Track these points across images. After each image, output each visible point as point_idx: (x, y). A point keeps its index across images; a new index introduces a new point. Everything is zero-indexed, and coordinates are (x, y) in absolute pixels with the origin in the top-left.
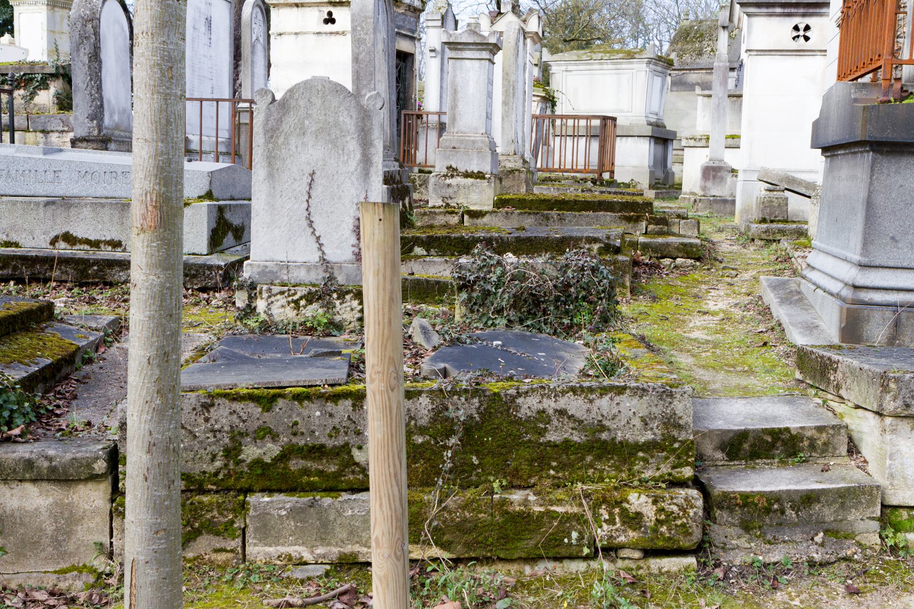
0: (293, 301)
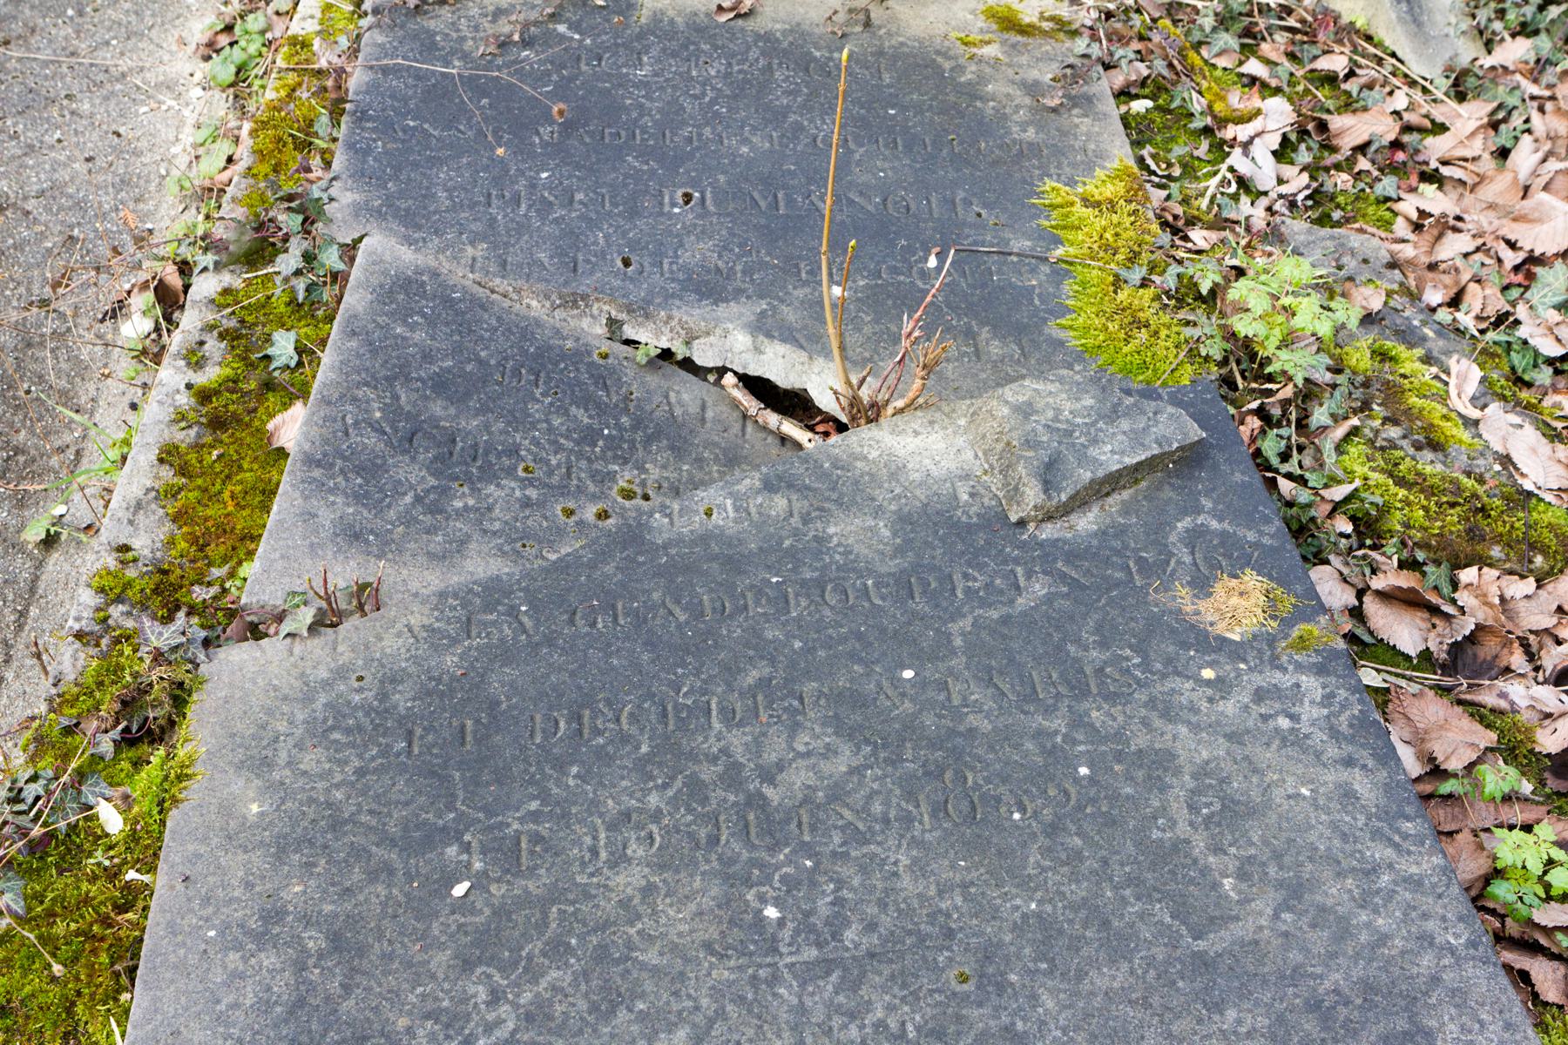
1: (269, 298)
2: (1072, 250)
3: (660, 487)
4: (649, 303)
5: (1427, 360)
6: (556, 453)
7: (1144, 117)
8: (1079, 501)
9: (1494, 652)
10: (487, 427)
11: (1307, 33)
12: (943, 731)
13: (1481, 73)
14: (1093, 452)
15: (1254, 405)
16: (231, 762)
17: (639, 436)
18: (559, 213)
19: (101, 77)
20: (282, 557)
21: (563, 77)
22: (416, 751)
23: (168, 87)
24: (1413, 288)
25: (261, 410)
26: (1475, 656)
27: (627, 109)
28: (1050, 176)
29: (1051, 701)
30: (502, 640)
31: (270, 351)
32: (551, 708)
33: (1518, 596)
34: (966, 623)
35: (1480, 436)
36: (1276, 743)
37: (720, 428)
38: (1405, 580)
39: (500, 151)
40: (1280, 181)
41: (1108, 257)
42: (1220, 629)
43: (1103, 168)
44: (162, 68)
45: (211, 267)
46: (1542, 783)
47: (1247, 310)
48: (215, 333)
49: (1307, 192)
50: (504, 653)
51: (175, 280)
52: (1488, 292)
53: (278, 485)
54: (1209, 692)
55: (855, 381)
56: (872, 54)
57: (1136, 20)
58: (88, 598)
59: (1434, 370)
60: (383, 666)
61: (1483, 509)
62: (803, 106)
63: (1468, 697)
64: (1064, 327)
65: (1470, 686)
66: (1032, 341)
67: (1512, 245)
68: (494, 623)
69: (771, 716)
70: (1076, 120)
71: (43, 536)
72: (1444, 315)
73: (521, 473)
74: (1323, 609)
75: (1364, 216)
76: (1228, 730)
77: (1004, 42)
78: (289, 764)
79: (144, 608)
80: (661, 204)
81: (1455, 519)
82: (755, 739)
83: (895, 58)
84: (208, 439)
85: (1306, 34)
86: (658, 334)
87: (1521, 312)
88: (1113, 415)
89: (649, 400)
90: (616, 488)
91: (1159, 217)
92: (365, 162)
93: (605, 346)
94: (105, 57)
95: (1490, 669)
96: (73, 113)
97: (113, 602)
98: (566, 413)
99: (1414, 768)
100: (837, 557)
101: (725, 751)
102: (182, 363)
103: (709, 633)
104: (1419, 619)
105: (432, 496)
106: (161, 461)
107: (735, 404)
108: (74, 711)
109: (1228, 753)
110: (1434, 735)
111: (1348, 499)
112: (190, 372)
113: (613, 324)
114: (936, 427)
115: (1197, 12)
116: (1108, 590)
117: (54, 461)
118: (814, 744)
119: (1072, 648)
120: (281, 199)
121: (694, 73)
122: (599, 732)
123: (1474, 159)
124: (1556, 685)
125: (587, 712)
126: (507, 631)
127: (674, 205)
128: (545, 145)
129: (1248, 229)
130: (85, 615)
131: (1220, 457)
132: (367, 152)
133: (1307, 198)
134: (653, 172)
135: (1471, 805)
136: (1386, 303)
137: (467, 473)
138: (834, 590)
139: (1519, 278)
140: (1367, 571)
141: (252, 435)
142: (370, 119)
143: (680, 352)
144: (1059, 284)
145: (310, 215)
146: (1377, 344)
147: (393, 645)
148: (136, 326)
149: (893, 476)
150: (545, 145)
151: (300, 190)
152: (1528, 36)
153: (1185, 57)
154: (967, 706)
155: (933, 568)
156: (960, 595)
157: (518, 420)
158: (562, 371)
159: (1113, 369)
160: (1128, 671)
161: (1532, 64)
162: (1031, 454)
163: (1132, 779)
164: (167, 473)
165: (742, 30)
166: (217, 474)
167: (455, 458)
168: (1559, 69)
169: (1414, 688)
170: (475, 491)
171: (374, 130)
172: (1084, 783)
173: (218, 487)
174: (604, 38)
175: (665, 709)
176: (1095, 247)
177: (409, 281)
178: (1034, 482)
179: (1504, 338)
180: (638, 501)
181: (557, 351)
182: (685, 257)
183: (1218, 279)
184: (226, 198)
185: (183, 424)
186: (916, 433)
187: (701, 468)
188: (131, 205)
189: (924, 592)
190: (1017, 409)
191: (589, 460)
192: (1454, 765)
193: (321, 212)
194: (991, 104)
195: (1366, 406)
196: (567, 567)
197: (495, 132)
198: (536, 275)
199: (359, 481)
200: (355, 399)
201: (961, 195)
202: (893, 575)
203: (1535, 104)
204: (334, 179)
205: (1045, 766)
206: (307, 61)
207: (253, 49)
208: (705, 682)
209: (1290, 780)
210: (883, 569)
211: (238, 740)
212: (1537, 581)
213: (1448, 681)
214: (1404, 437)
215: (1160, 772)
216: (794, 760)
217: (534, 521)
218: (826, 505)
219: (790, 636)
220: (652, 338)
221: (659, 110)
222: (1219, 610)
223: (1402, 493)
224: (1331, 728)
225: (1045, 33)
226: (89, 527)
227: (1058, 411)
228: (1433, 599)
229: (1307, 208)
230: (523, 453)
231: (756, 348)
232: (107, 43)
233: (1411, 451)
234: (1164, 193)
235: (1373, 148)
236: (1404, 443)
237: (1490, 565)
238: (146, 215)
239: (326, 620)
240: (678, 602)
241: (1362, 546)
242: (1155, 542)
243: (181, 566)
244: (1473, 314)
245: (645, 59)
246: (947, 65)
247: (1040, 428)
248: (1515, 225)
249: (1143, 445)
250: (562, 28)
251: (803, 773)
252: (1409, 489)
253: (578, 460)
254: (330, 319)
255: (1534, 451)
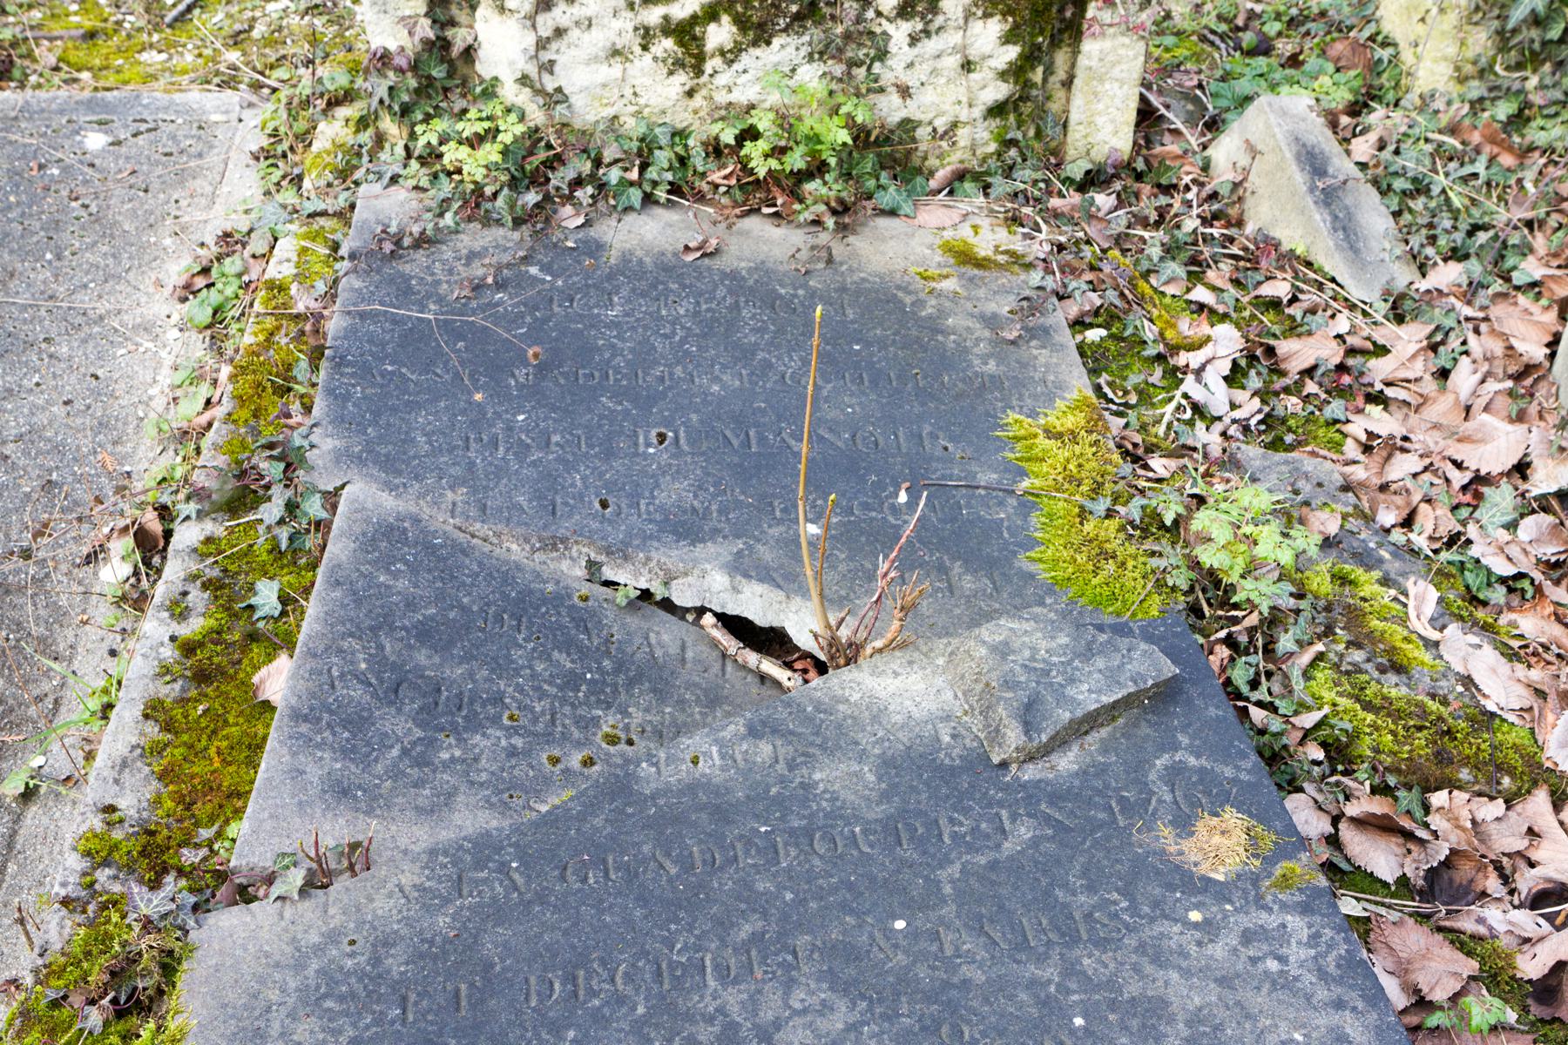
0: (670, 28)
1: (251, 546)
2: (1038, 483)
3: (643, 731)
4: (628, 545)
5: (1385, 582)
6: (540, 699)
7: (1100, 346)
8: (1059, 742)
9: (1469, 876)
10: (471, 675)
11: (1251, 260)
12: (937, 984)
13: (1417, 297)
14: (1070, 691)
15: (1222, 634)
16: (222, 1035)
17: (621, 678)
18: (536, 455)
19: (80, 320)
20: (271, 816)
21: (536, 319)
22: (411, 1018)
23: (145, 329)
24: (1367, 511)
25: (246, 662)
26: (1451, 880)
27: (599, 349)
28: (1012, 408)
29: (1041, 949)
30: (494, 899)
31: (253, 601)
32: (545, 970)
33: (1489, 818)
34: (955, 870)
35: (1441, 657)
36: (1266, 987)
37: (700, 668)
38: (1378, 806)
39: (478, 397)
40: (1233, 406)
41: (1072, 488)
42: (1204, 869)
43: (1064, 399)
44: (139, 311)
45: (194, 516)
46: (1525, 1009)
47: (1210, 540)
48: (198, 583)
49: (1260, 417)
50: (497, 913)
51: (155, 526)
52: (1439, 512)
53: (265, 739)
54: (1198, 935)
55: (833, 623)
56: (836, 290)
57: (1087, 252)
58: (75, 862)
59: (1393, 592)
60: (375, 929)
61: (1449, 732)
62: (771, 343)
63: (1447, 924)
64: (1033, 560)
65: (1449, 912)
66: (1004, 574)
67: (1459, 465)
68: (485, 881)
69: (766, 972)
70: (1035, 352)
71: (22, 789)
72: (1398, 536)
73: (506, 721)
74: (1303, 843)
75: (1315, 438)
76: (1218, 974)
77: (961, 276)
78: (282, 1034)
79: (131, 871)
80: (636, 444)
81: (1423, 742)
82: (751, 997)
83: (858, 292)
84: (193, 693)
85: (1249, 260)
86: (637, 575)
87: (1472, 531)
88: (1088, 653)
89: (630, 642)
90: (600, 735)
91: (1119, 446)
92: (344, 407)
93: (586, 588)
94: (83, 300)
95: (1467, 894)
96: (51, 356)
97: (99, 865)
98: (549, 658)
99: (1400, 1000)
100: (824, 804)
101: (721, 1010)
102: (166, 614)
103: (701, 886)
104: (1394, 844)
105: (418, 749)
106: (146, 716)
107: (715, 644)
108: (61, 983)
109: (1220, 999)
110: (1417, 966)
111: (1319, 725)
112: (174, 624)
113: (593, 566)
114: (915, 667)
115: (1144, 241)
116: (1093, 832)
117: (32, 711)
118: (810, 1000)
119: (1059, 893)
120: (263, 447)
121: (664, 312)
122: (595, 994)
123: (1416, 380)
124: (1532, 909)
125: (582, 973)
126: (499, 889)
127: (648, 445)
128: (520, 387)
129: (1206, 456)
130: (71, 880)
131: (1193, 692)
132: (346, 397)
133: (1260, 422)
134: (627, 412)
135: (1458, 1036)
136: (1342, 526)
137: (453, 723)
138: (822, 838)
139: (1467, 498)
140: (1341, 797)
141: (236, 687)
142: (349, 364)
143: (659, 592)
144: (1026, 516)
145: (291, 462)
146: (1336, 569)
147: (384, 906)
148: (116, 571)
149: (875, 719)
150: (520, 387)
151: (281, 437)
152: (1459, 260)
153: (1135, 286)
154: (959, 956)
155: (920, 813)
156: (947, 840)
157: (501, 667)
158: (543, 615)
159: (1083, 601)
160: (1116, 915)
161: (1465, 287)
162: (1010, 695)
163: (1127, 1028)
164: (152, 729)
165: (709, 269)
166: (202, 729)
167: (440, 708)
168: (1490, 291)
169: (1394, 916)
170: (461, 741)
171: (353, 375)
172: (1080, 1034)
173: (204, 743)
174: (575, 279)
175: (659, 967)
176: (1060, 478)
177: (391, 528)
178: (1015, 724)
179: (1457, 558)
180: (623, 747)
181: (538, 595)
182: (662, 497)
183: (1181, 510)
184: (206, 443)
185: (168, 678)
186: (896, 674)
187: (683, 710)
188: (109, 447)
189: (911, 839)
190: (994, 649)
191: (572, 705)
192: (1439, 995)
193: (303, 460)
194: (952, 337)
195: (1329, 631)
196: (556, 820)
197: (471, 376)
198: (515, 519)
199: (346, 735)
200: (340, 651)
201: (927, 429)
202: (880, 821)
203: (1470, 326)
204: (314, 425)
205: (1041, 1018)
206: (285, 305)
207: (229, 292)
208: (698, 938)
209: (1283, 1026)
210: (871, 816)
211: (230, 1011)
212: (1506, 802)
213: (1426, 908)
214: (1368, 660)
215: (1154, 1021)
216: (790, 1018)
217: (521, 771)
218: (811, 750)
219: (781, 888)
220: (631, 578)
221: (632, 350)
222: (1202, 849)
223: (1370, 717)
224: (1319, 970)
225: (1000, 266)
226: (68, 778)
227: (1034, 650)
228: (1406, 824)
229: (1260, 433)
230: (507, 701)
231: (734, 588)
232: (85, 286)
233: (1376, 674)
234: (1122, 421)
235: (1320, 372)
236: (1369, 667)
237: (1460, 788)
238: (124, 458)
239: (317, 881)
240: (668, 855)
241: (1334, 772)
242: (1136, 781)
243: (168, 827)
244: (1426, 535)
245: (616, 299)
246: (908, 300)
247: (1018, 668)
248: (1459, 446)
249: (1118, 683)
250: (534, 270)
251: (800, 1031)
252: (1377, 714)
253: (561, 706)
254: (313, 566)
255: (1494, 671)
